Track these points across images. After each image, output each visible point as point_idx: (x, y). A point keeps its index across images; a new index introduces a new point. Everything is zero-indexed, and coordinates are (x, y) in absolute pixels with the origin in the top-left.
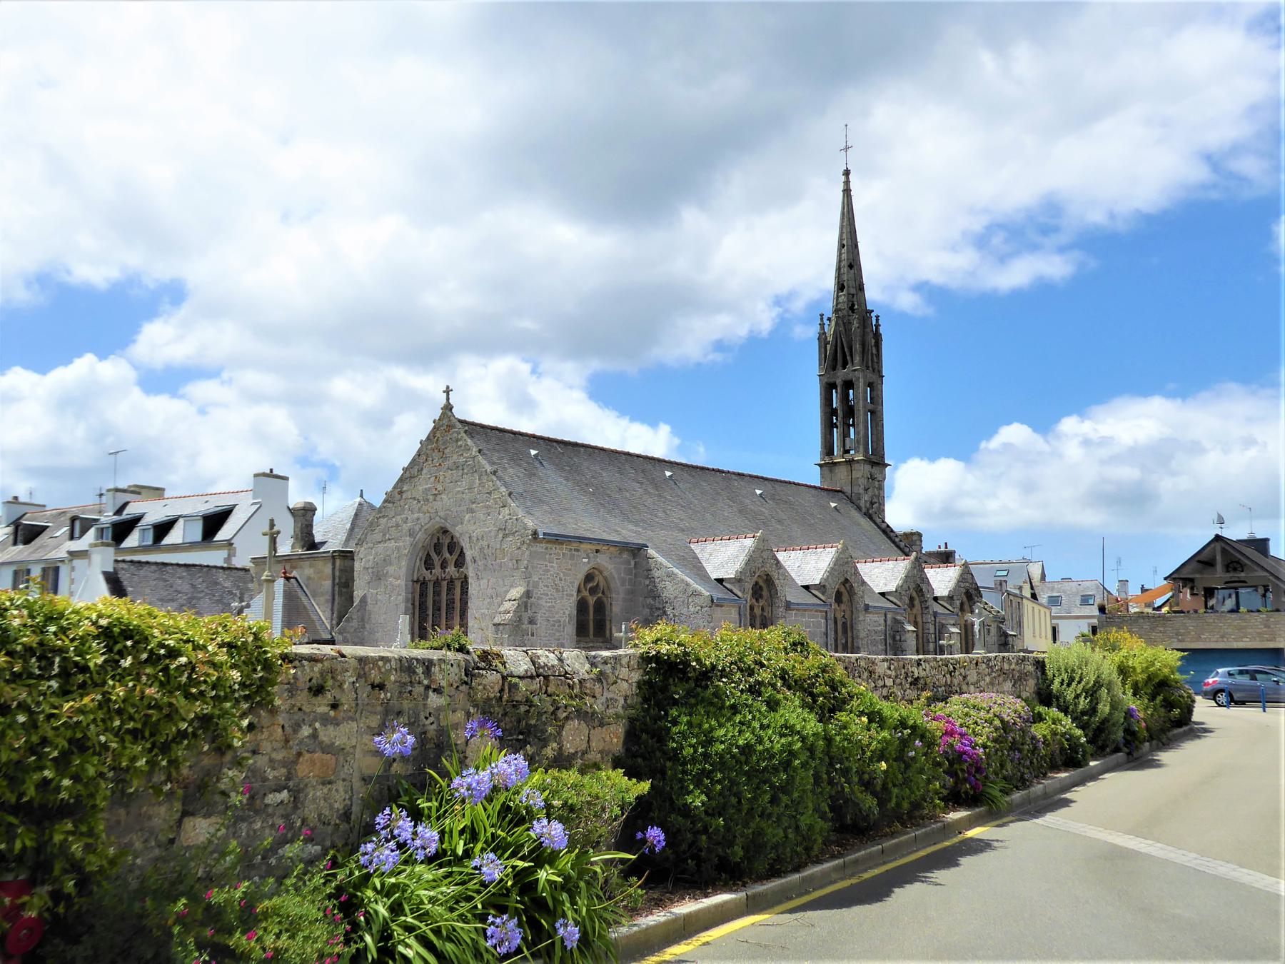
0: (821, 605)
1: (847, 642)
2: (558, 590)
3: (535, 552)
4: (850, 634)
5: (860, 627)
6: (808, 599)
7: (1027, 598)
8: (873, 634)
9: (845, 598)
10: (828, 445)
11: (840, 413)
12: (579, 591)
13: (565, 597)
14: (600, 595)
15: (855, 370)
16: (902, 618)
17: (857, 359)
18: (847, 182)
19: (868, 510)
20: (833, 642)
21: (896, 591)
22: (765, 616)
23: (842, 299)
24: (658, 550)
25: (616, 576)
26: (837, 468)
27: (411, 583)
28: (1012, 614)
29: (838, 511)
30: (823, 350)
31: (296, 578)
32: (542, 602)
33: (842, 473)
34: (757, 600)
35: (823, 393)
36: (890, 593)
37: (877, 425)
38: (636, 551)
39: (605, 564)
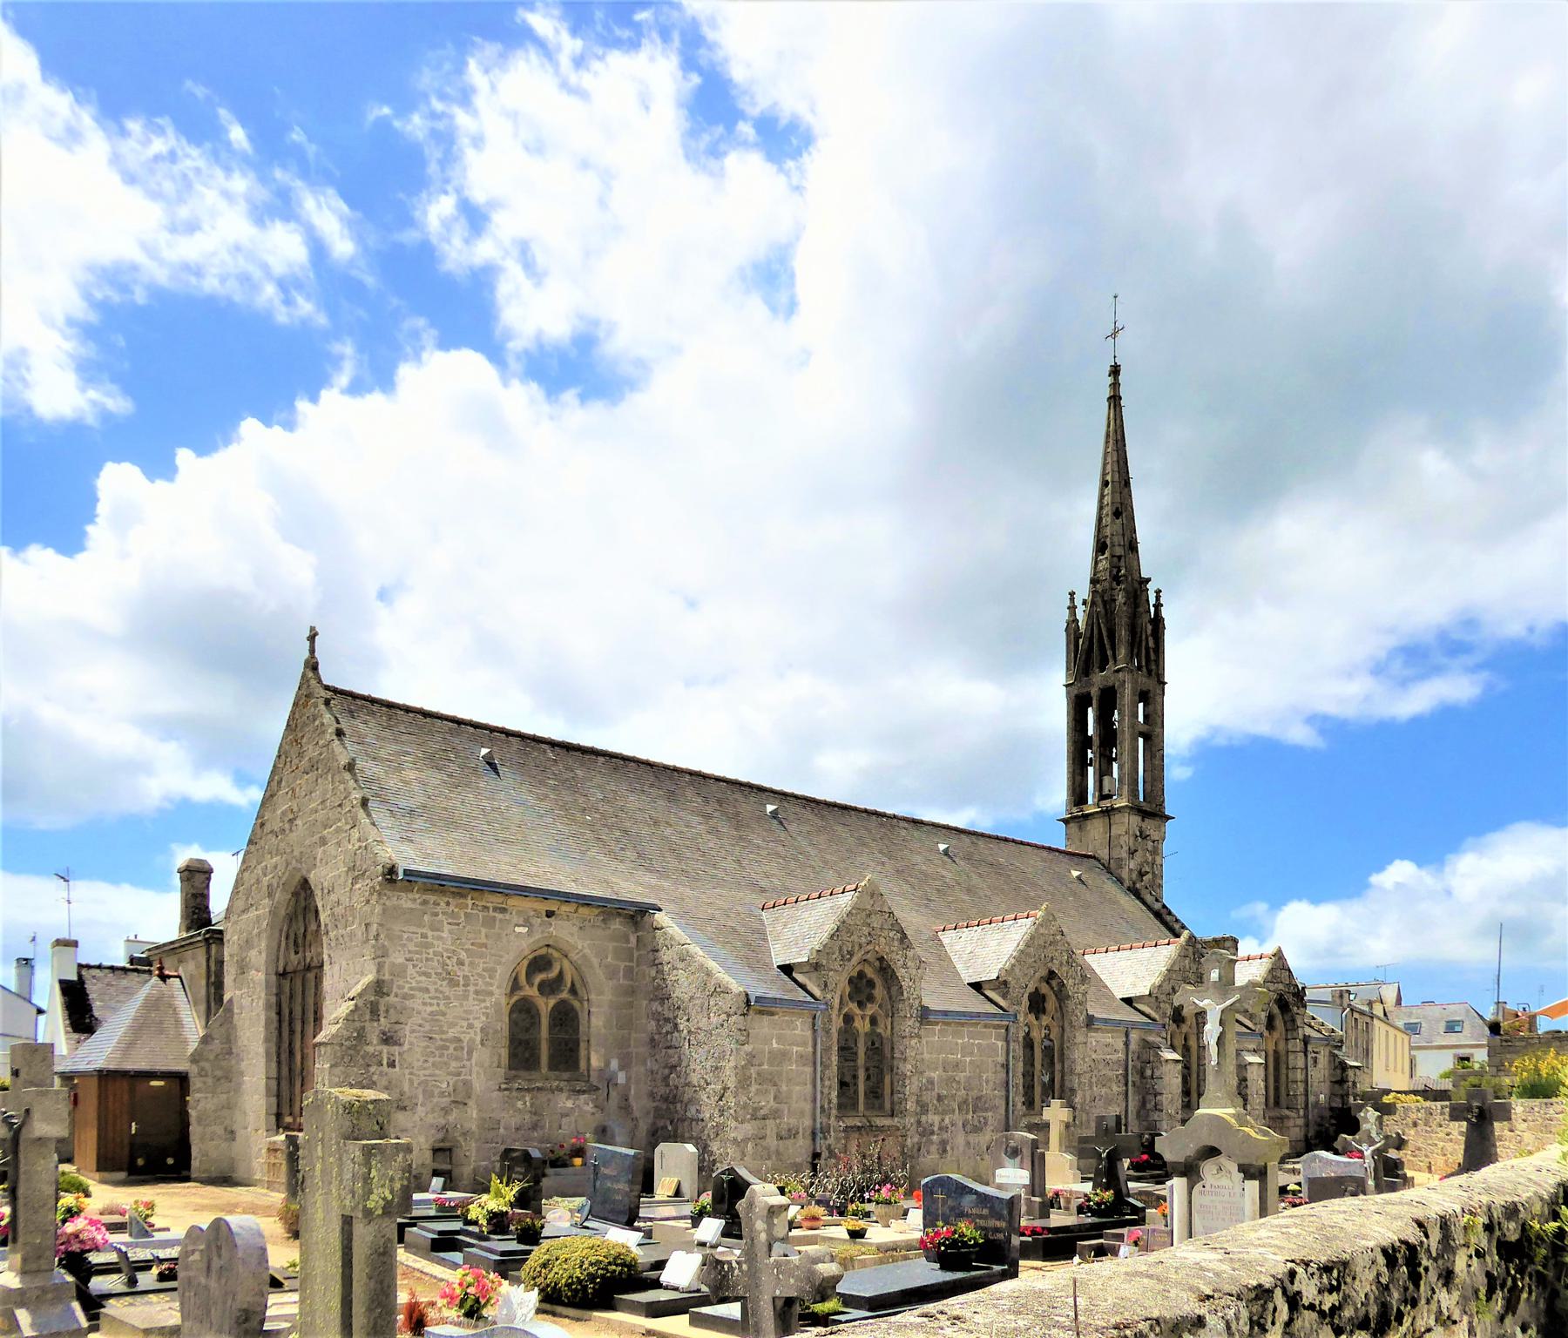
0: (994, 1015)
1: (1052, 1080)
2: (453, 983)
3: (395, 908)
4: (1058, 1067)
5: (1077, 1054)
6: (976, 1004)
7: (1379, 1018)
9: (1051, 1004)
10: (1078, 790)
11: (1096, 741)
12: (515, 986)
13: (472, 996)
14: (565, 995)
15: (1118, 671)
17: (1122, 652)
18: (1115, 385)
19: (1134, 883)
20: (1020, 1080)
23: (1103, 565)
24: (683, 916)
25: (595, 961)
26: (1088, 822)
27: (274, 978)
28: (1356, 1039)
29: (1083, 883)
30: (1072, 647)
31: (179, 977)
32: (415, 1004)
33: (1096, 829)
34: (861, 1005)
36: (1140, 998)
37: (1153, 756)
38: (637, 915)
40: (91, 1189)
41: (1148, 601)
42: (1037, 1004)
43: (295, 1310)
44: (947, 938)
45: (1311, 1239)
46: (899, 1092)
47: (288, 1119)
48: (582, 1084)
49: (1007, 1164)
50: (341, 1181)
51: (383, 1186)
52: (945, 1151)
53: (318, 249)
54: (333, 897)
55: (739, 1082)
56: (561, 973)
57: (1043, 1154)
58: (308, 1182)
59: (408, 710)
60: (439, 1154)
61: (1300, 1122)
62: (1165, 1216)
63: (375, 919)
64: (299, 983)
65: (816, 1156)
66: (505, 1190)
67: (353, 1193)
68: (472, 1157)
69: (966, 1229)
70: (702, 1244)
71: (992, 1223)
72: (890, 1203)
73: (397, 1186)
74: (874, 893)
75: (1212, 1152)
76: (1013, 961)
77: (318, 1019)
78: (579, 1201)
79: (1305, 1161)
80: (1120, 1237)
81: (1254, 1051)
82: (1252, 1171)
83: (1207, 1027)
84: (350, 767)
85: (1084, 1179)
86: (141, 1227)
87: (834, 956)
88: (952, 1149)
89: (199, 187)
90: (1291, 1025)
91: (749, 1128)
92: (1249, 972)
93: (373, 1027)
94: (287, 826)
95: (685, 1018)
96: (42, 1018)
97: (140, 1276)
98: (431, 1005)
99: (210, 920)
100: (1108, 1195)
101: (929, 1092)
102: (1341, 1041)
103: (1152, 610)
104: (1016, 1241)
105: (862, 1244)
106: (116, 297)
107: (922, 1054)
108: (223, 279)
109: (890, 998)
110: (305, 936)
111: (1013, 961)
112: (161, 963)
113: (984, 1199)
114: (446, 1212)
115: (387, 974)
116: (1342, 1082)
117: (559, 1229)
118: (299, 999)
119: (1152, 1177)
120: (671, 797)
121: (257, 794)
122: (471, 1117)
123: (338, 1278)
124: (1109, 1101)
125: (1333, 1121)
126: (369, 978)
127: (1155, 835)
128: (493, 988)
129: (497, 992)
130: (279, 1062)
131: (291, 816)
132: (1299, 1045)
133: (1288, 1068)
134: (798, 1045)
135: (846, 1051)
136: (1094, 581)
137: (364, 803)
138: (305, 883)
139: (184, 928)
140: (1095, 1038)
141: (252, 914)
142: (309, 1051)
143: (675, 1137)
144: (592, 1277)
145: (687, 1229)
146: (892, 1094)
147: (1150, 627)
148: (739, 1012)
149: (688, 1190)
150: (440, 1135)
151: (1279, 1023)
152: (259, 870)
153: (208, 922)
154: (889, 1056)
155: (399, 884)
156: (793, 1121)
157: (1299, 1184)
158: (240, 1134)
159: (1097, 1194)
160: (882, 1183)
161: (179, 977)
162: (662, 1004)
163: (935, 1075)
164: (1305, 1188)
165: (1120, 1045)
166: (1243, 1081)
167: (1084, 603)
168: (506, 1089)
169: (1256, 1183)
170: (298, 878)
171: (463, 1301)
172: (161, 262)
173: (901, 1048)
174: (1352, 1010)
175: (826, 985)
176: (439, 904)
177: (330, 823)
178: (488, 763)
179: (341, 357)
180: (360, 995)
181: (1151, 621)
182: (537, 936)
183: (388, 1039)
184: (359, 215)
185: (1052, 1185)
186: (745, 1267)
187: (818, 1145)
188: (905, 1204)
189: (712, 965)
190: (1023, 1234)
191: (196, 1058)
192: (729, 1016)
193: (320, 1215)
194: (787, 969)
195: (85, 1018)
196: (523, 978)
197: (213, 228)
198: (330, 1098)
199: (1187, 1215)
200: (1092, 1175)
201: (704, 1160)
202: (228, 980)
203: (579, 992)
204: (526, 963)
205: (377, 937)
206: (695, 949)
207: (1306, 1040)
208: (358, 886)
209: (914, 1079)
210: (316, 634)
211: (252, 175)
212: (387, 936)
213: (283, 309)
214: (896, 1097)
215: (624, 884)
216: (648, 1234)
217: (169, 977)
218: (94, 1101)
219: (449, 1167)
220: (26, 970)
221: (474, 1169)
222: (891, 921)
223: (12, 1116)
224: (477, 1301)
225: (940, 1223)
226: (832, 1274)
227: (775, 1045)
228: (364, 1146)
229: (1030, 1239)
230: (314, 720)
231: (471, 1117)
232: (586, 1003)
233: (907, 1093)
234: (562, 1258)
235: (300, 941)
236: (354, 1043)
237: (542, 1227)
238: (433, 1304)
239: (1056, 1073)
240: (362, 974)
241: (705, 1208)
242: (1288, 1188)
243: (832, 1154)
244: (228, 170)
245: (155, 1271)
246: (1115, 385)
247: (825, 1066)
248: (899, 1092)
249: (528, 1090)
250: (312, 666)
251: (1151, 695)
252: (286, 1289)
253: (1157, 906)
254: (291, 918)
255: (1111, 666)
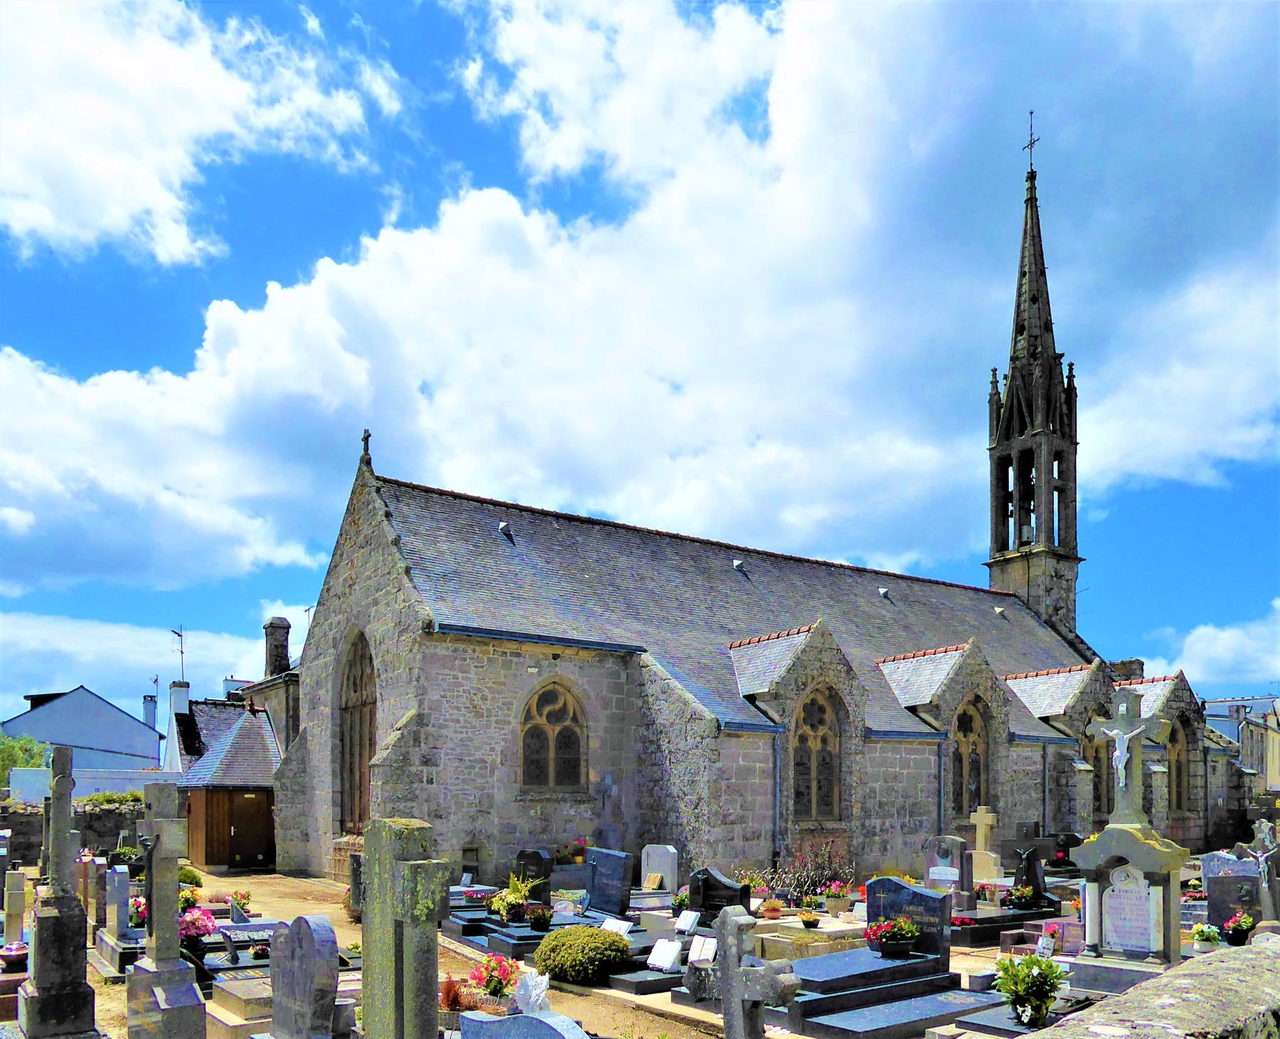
1: (978, 789)
2: (479, 715)
4: (983, 777)
5: (999, 766)
6: (911, 724)
7: (1273, 730)
8: (1022, 776)
9: (977, 723)
11: (1016, 496)
12: (528, 717)
13: (494, 725)
14: (568, 723)
15: (1035, 435)
16: (1071, 753)
17: (1039, 419)
18: (1032, 189)
19: (1050, 616)
20: (950, 789)
21: (1065, 714)
22: (829, 752)
23: (1022, 343)
27: (337, 712)
31: (265, 711)
33: (1017, 571)
34: (813, 727)
35: (994, 472)
36: (1056, 717)
37: (1067, 507)
38: (628, 655)
39: (572, 677)
40: (202, 881)
41: (1061, 373)
42: (965, 723)
43: (359, 986)
44: (886, 669)
45: (1208, 1006)
46: (846, 800)
47: (350, 825)
48: (581, 796)
49: (939, 864)
50: (394, 893)
51: (426, 898)
52: (885, 849)
53: (372, 108)
54: (384, 647)
55: (712, 793)
56: (565, 704)
57: (971, 855)
58: (368, 893)
59: (442, 493)
60: (469, 853)
61: (1201, 822)
62: (1078, 910)
63: (417, 665)
64: (357, 716)
65: (776, 854)
66: (521, 886)
67: (403, 902)
68: (493, 856)
69: (904, 924)
70: (681, 932)
71: (927, 919)
72: (839, 897)
73: (438, 897)
74: (824, 633)
75: (1121, 861)
76: (944, 688)
77: (372, 744)
78: (582, 893)
79: (1204, 860)
80: (1039, 928)
81: (1159, 761)
82: (1157, 878)
83: (1117, 753)
84: (396, 542)
85: (1007, 875)
86: (241, 916)
87: (791, 687)
88: (892, 848)
89: (280, 69)
90: (1192, 738)
91: (719, 832)
92: (1153, 698)
93: (415, 752)
94: (347, 590)
95: (667, 741)
96: (163, 743)
97: (241, 954)
98: (461, 732)
99: (289, 665)
100: (1028, 891)
101: (872, 800)
102: (1238, 751)
103: (1066, 381)
104: (947, 931)
105: (815, 933)
106: (218, 159)
107: (866, 767)
108: (297, 140)
109: (838, 721)
110: (361, 678)
111: (944, 688)
112: (251, 701)
113: (918, 898)
114: (476, 902)
115: (426, 709)
116: (1238, 787)
117: (566, 917)
118: (357, 727)
119: (1067, 872)
120: (654, 556)
121: (325, 559)
122: (492, 824)
123: (393, 969)
124: (1028, 806)
125: (1231, 822)
126: (412, 712)
127: (1069, 575)
128: (511, 719)
129: (513, 721)
130: (342, 779)
131: (351, 583)
132: (1199, 756)
133: (1189, 776)
134: (760, 762)
135: (802, 766)
136: (1013, 359)
137: (408, 571)
138: (362, 636)
139: (268, 672)
140: (1015, 752)
141: (322, 661)
142: (366, 770)
143: (659, 840)
144: (592, 960)
145: (669, 918)
146: (840, 802)
147: (1063, 396)
148: (712, 735)
149: (670, 883)
150: (467, 839)
151: (1181, 736)
152: (326, 627)
153: (287, 668)
154: (838, 770)
155: (435, 635)
156: (756, 826)
157: (1199, 879)
158: (312, 835)
159: (1018, 890)
160: (832, 879)
161: (265, 711)
162: (647, 729)
163: (877, 786)
164: (1205, 883)
165: (1038, 758)
166: (1148, 787)
167: (1006, 377)
168: (520, 801)
169: (1161, 888)
170: (356, 632)
171: (489, 982)
172: (250, 129)
173: (849, 763)
174: (1247, 723)
175: (784, 711)
176: (467, 651)
177: (382, 587)
178: (505, 534)
179: (391, 198)
180: (405, 726)
181: (1065, 390)
182: (546, 675)
183: (426, 762)
184: (406, 80)
185: (979, 879)
186: (719, 974)
187: (777, 845)
188: (851, 897)
189: (689, 696)
190: (953, 925)
191: (279, 775)
192: (703, 738)
193: (378, 920)
194: (751, 699)
195: (195, 743)
196: (534, 707)
197: (290, 99)
198: (385, 827)
199: (1097, 916)
200: (1014, 871)
201: (682, 857)
202: (303, 712)
203: (580, 721)
204: (536, 697)
205: (418, 680)
206: (674, 683)
207: (1206, 751)
208: (403, 638)
209: (859, 789)
210: (370, 435)
211: (321, 54)
212: (427, 678)
213: (344, 162)
214: (844, 804)
215: (615, 631)
216: (636, 921)
217: (258, 711)
218: (203, 810)
219: (476, 864)
220: (152, 704)
221: (496, 867)
222: (840, 656)
223: (146, 840)
224: (500, 982)
225: (882, 919)
226: (791, 983)
227: (741, 762)
228: (412, 866)
229: (960, 929)
230: (368, 505)
231: (492, 824)
232: (585, 729)
233: (853, 801)
234: (567, 944)
235: (358, 681)
236: (401, 764)
237: (551, 916)
238: (464, 981)
239: (982, 782)
240: (407, 709)
241: (684, 901)
242: (1189, 883)
243: (790, 853)
244: (302, 52)
245: (251, 951)
246: (1032, 189)
247: (783, 779)
248: (846, 800)
249: (539, 801)
250: (367, 461)
251: (1065, 451)
252: (351, 967)
253: (1071, 636)
254: (351, 664)
255: (1029, 432)
